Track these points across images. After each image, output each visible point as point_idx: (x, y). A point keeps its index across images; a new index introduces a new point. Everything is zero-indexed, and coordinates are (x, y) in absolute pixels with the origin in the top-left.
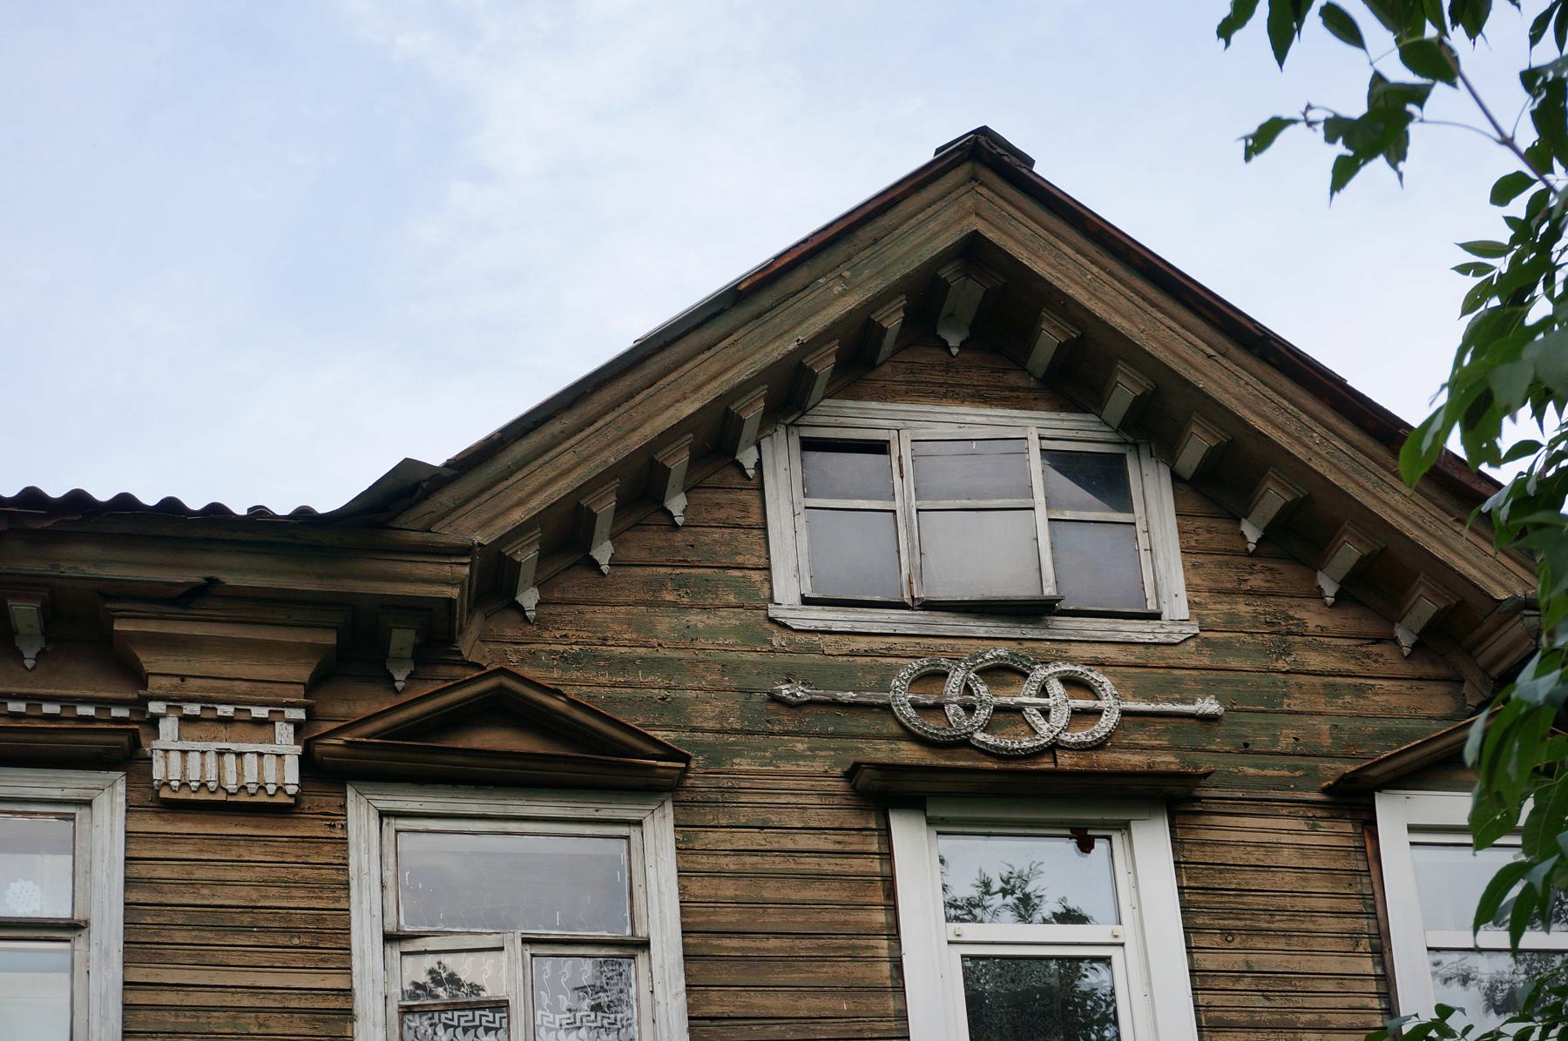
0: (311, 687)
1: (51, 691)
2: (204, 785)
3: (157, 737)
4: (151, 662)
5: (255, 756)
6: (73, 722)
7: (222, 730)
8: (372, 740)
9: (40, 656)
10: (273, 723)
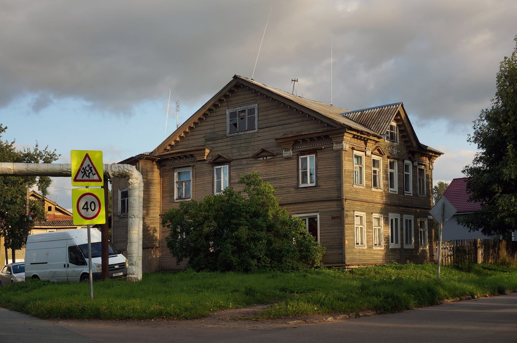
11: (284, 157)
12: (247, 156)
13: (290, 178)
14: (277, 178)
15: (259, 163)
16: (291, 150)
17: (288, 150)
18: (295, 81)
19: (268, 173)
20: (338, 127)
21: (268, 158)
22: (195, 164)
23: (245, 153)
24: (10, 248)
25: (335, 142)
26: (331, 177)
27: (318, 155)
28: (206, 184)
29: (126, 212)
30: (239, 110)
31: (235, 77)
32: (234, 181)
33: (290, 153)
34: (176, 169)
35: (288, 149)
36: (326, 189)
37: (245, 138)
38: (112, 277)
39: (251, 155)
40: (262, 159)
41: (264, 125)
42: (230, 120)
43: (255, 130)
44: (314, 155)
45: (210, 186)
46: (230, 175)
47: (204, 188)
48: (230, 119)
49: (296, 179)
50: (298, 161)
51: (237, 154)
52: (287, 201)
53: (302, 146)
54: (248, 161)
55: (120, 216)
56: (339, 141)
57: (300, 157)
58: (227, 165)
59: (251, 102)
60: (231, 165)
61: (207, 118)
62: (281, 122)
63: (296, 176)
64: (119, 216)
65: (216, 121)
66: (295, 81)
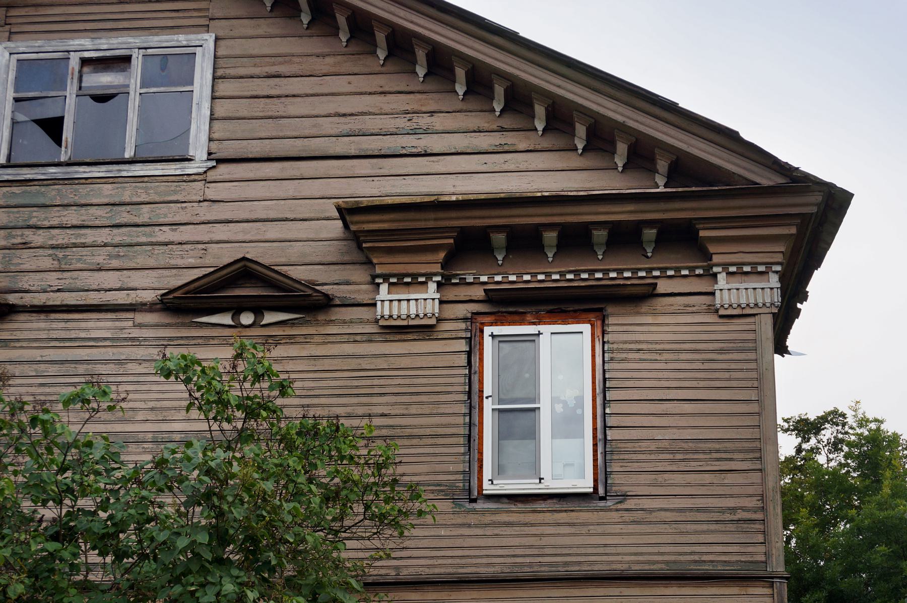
0: (445, 265)
1: (598, 268)
2: (739, 306)
3: (379, 294)
4: (712, 249)
5: (769, 289)
6: (507, 284)
7: (404, 289)
8: (188, 295)
9: (604, 254)
10: (768, 273)
11: (382, 323)
13: (420, 437)
16: (432, 286)
17: (415, 281)
18: (208, 422)
20: (766, 179)
21: (270, 317)
24: (562, 410)
25: (725, 266)
27: (610, 329)
30: (87, 55)
36: (668, 514)
38: (824, 192)
39: (149, 296)
40: (226, 319)
42: (17, 100)
43: (186, 164)
44: (586, 328)
48: (16, 91)
49: (462, 450)
52: (397, 568)
56: (754, 264)
57: (488, 330)
59: (170, 23)
63: (464, 431)
66: (208, 422)
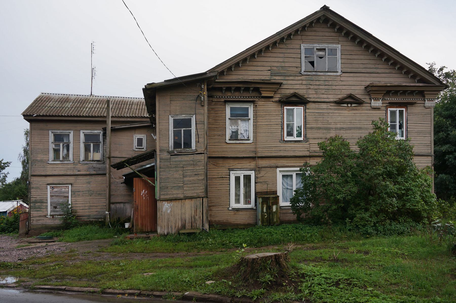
12: (327, 100)
14: (363, 128)
15: (342, 109)
16: (381, 100)
19: (353, 122)
21: (353, 105)
22: (256, 100)
23: (325, 96)
26: (421, 133)
28: (273, 126)
29: (183, 148)
31: (325, 8)
32: (311, 126)
33: (379, 103)
34: (229, 104)
35: (378, 98)
37: (325, 80)
41: (349, 70)
42: (305, 57)
43: (337, 73)
45: (279, 129)
46: (305, 119)
47: (269, 130)
50: (386, 113)
51: (315, 96)
53: (392, 98)
54: (329, 105)
55: (173, 152)
57: (389, 109)
58: (302, 106)
60: (307, 107)
61: (273, 48)
62: (369, 70)
64: (169, 152)
65: (286, 54)
